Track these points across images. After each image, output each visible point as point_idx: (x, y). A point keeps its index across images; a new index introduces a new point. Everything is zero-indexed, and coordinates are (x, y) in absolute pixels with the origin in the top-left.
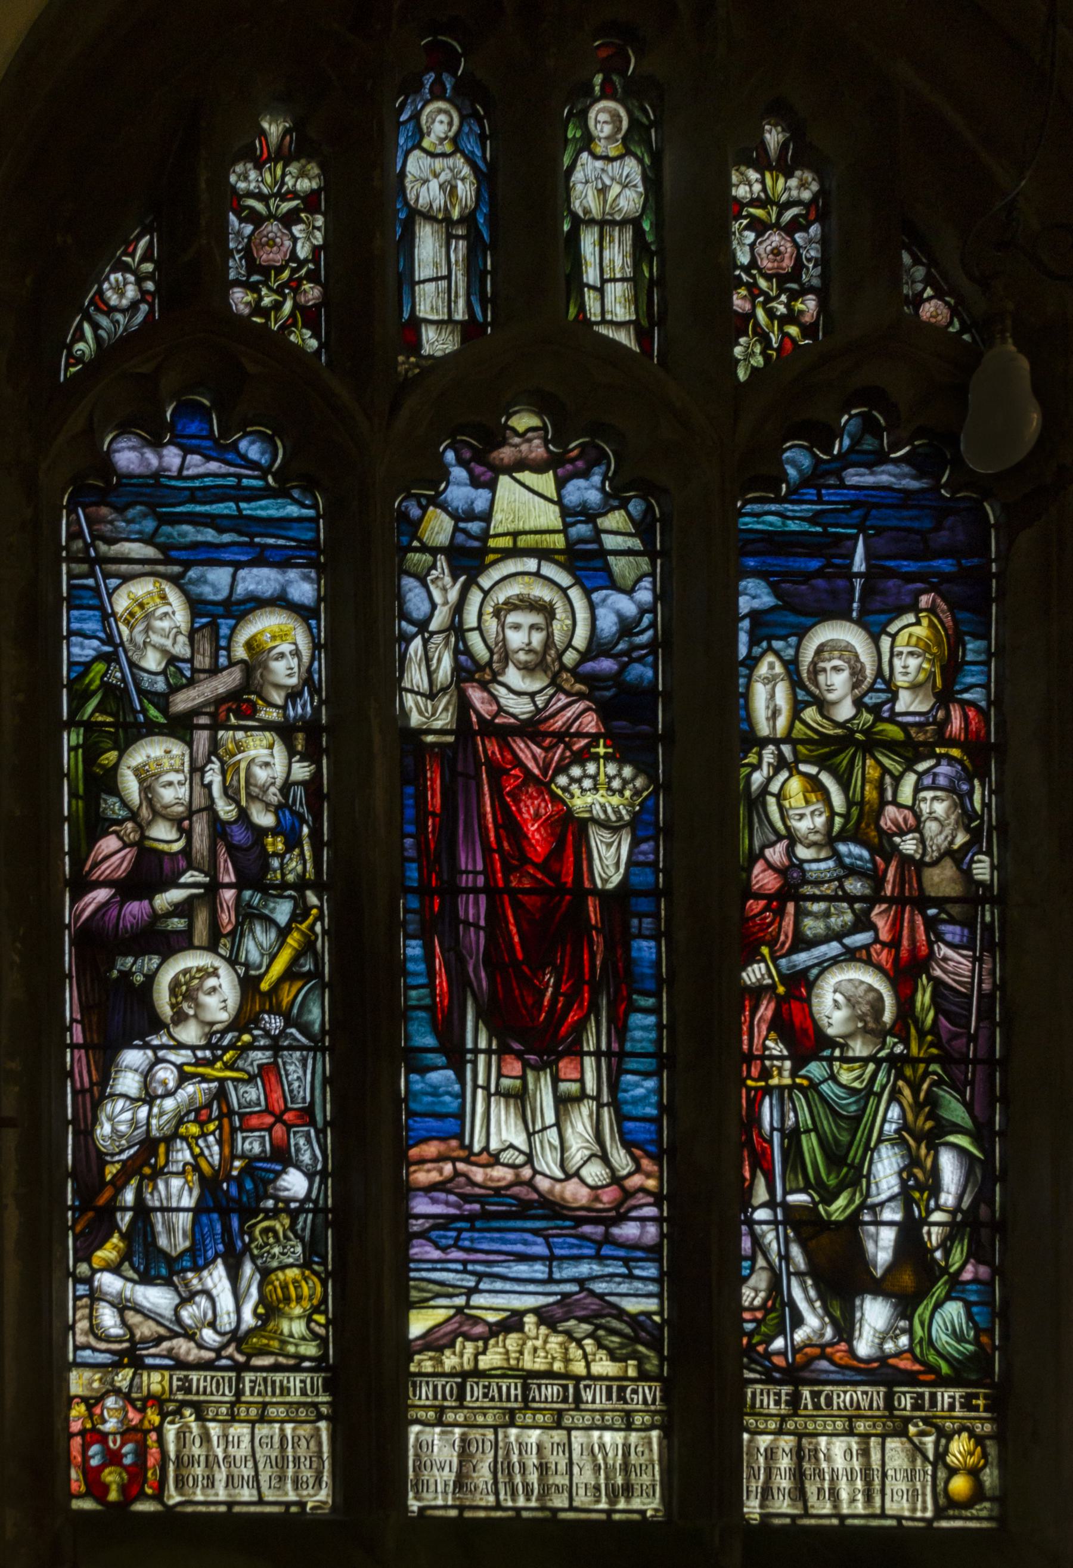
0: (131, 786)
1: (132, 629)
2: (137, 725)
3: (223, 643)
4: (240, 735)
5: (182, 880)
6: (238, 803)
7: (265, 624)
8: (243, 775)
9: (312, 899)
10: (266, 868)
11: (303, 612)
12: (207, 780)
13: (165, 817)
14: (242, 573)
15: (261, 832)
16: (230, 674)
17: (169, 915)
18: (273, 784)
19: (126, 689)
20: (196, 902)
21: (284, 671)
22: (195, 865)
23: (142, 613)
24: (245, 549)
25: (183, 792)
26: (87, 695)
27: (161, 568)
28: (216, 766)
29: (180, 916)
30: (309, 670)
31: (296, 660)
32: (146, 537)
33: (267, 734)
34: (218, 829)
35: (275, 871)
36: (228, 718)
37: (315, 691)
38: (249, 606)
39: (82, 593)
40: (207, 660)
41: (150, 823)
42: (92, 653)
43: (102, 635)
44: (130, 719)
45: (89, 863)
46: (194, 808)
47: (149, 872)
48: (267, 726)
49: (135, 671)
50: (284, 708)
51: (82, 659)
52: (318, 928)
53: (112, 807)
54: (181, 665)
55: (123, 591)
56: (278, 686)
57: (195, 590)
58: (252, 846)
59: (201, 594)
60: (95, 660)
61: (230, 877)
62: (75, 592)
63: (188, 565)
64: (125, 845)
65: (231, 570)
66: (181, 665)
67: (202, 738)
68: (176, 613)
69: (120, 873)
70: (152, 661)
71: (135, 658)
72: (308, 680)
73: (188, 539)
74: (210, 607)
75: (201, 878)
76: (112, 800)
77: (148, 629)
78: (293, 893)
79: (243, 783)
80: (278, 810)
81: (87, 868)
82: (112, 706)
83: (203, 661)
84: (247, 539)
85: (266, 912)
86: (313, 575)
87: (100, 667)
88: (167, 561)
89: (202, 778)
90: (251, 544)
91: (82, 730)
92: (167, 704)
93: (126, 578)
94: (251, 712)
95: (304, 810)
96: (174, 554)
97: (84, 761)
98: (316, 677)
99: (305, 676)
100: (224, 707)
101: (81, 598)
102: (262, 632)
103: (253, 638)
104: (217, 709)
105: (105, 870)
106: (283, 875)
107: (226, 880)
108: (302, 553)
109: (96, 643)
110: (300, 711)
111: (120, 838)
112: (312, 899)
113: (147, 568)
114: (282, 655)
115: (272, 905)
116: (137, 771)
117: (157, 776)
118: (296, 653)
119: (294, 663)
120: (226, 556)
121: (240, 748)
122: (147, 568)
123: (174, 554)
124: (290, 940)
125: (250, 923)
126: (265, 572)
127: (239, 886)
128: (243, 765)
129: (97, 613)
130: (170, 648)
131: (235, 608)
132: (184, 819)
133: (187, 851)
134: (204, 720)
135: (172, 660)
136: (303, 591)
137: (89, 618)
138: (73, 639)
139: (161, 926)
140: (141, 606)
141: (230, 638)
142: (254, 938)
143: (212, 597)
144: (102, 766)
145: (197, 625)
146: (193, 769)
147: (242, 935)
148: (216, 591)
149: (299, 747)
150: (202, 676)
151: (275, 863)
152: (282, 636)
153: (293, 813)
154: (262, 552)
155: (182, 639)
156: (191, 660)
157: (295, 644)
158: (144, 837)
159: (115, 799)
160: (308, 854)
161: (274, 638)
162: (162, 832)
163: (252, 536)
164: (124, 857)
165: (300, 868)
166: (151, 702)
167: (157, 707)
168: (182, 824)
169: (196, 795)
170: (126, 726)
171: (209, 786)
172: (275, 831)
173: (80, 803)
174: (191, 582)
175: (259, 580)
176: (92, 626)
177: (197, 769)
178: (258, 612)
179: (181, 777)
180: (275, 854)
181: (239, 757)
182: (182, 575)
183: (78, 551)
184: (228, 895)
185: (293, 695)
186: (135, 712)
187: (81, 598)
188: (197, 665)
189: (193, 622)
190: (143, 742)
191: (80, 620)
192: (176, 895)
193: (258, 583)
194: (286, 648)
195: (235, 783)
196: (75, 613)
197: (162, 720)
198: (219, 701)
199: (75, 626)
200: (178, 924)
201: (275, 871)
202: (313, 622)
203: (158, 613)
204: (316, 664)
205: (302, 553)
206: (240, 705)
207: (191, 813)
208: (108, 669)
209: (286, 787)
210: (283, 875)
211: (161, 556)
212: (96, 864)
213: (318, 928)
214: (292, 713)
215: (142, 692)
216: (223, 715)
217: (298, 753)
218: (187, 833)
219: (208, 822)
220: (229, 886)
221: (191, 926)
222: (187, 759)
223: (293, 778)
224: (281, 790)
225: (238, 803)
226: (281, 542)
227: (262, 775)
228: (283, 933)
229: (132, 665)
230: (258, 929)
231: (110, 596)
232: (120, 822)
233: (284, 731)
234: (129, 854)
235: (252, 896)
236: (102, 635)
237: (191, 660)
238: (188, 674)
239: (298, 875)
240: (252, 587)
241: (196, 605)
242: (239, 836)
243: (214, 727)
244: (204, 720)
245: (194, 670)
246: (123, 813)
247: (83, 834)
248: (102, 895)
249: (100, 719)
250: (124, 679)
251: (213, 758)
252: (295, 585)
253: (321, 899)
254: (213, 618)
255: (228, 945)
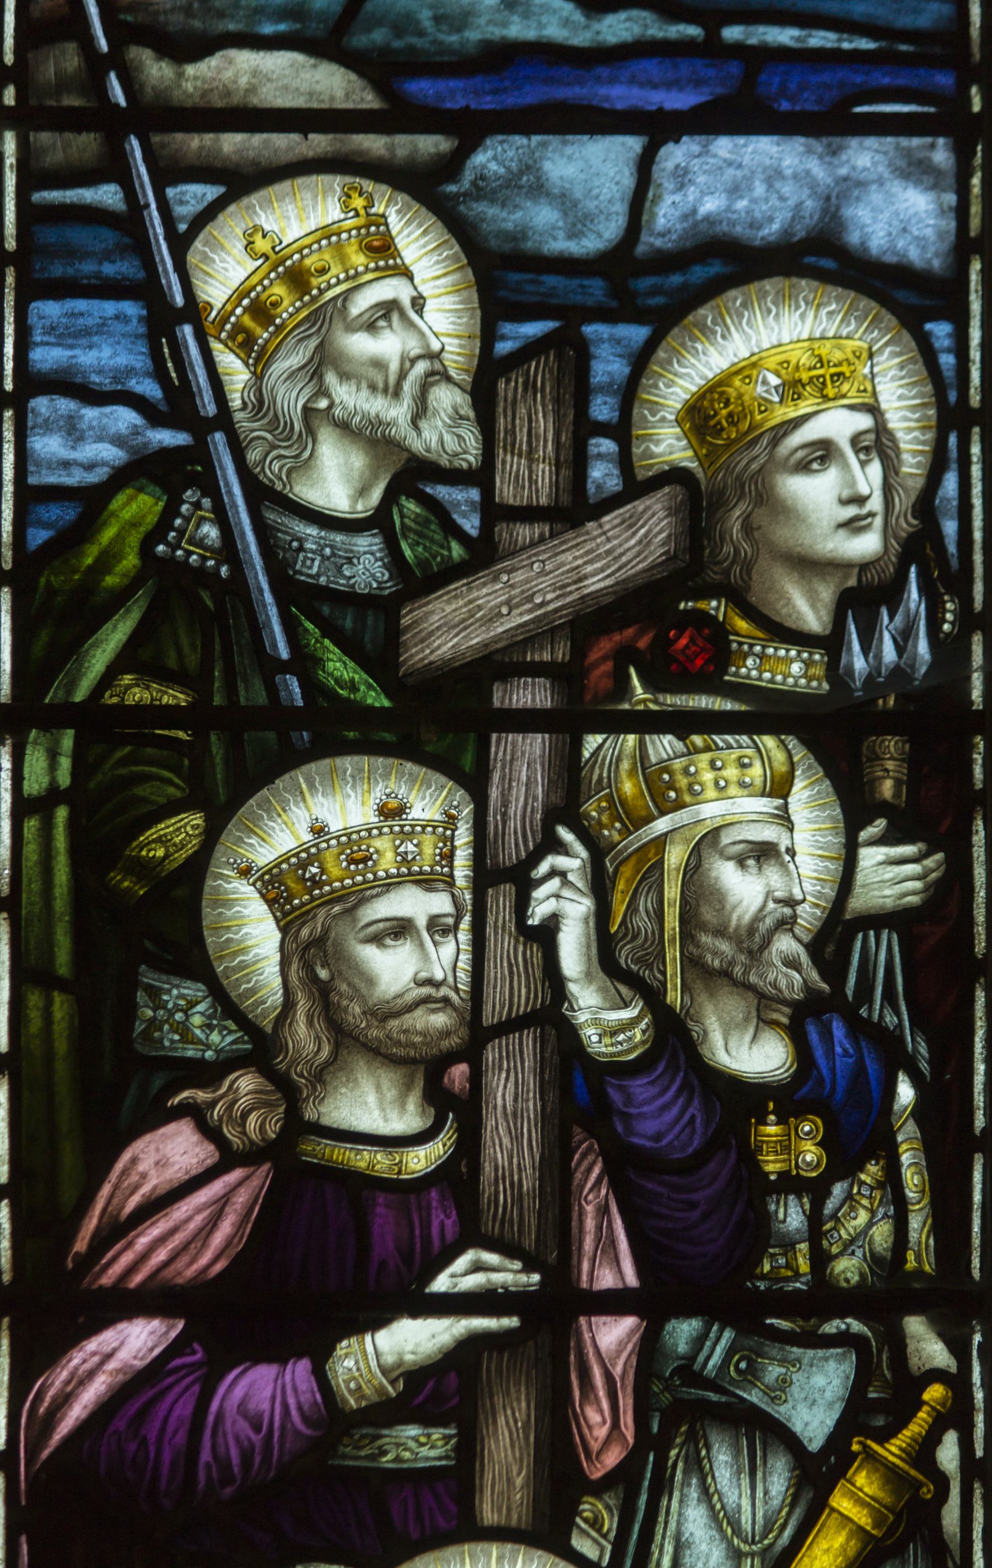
0: (254, 935)
1: (259, 361)
2: (277, 714)
3: (603, 409)
4: (663, 746)
5: (441, 1284)
6: (653, 998)
7: (764, 337)
8: (672, 891)
9: (928, 1347)
10: (758, 1233)
11: (901, 294)
12: (539, 912)
13: (383, 1055)
14: (675, 155)
15: (743, 1100)
16: (630, 524)
17: (387, 1412)
18: (786, 924)
19: (239, 584)
20: (489, 1364)
21: (832, 508)
22: (490, 1227)
23: (301, 304)
24: (685, 68)
25: (448, 958)
26: (90, 612)
27: (374, 144)
28: (574, 861)
29: (427, 1421)
30: (925, 506)
31: (875, 469)
32: (315, 29)
33: (769, 742)
34: (578, 1089)
35: (789, 1245)
36: (623, 689)
37: (946, 580)
38: (699, 273)
39: (78, 235)
40: (544, 473)
41: (321, 1077)
42: (111, 454)
43: (150, 389)
44: (253, 694)
45: (91, 1224)
46: (489, 1017)
47: (322, 1247)
48: (769, 713)
49: (271, 516)
50: (832, 643)
51: (74, 478)
52: (948, 1454)
53: (184, 1017)
54: (442, 492)
55: (231, 227)
56: (810, 566)
57: (496, 218)
58: (701, 1158)
59: (521, 234)
60: (122, 477)
61: (617, 1271)
62: (48, 235)
63: (470, 130)
64: (229, 1156)
65: (634, 144)
66: (442, 492)
67: (523, 763)
68: (426, 300)
69: (209, 1259)
70: (335, 481)
71: (272, 471)
72: (919, 544)
73: (473, 35)
74: (552, 281)
75: (508, 1275)
76: (182, 991)
77: (324, 361)
78: (856, 1326)
79: (672, 921)
80: (800, 1020)
81: (81, 1245)
82: (185, 647)
83: (528, 477)
84: (693, 31)
85: (754, 1397)
86: (942, 155)
87: (138, 506)
88: (398, 116)
89: (522, 904)
90: (710, 48)
91: (67, 740)
92: (393, 638)
93: (242, 182)
94: (710, 659)
95: (897, 1019)
96: (422, 89)
97: (73, 851)
98: (950, 528)
99: (907, 525)
100: (605, 646)
101: (72, 254)
102: (746, 370)
103: (715, 389)
104: (579, 651)
105: (148, 1251)
106: (820, 1259)
107: (606, 1280)
108: (903, 80)
109: (124, 418)
110: (889, 653)
111: (209, 1132)
112: (928, 1347)
113: (320, 143)
114: (824, 452)
115: (774, 1372)
116: (274, 886)
117: (353, 899)
118: (877, 443)
119: (870, 478)
120: (620, 94)
121: (664, 793)
122: (322, 143)
123: (422, 89)
124: (841, 1502)
125: (693, 1438)
126: (763, 149)
127: (651, 1304)
128: (675, 856)
129: (131, 309)
130: (403, 430)
131: (645, 283)
132: (451, 1058)
133: (460, 1174)
134: (530, 695)
135: (412, 475)
136: (902, 213)
137: (101, 328)
138: (41, 405)
139: (352, 1455)
140: (298, 279)
141: (629, 392)
142: (706, 1494)
143: (560, 245)
144: (143, 869)
145: (503, 348)
146: (486, 875)
147: (661, 1486)
148: (578, 223)
149: (887, 788)
150: (524, 532)
151: (792, 1216)
152: (818, 381)
153: (861, 1029)
154: (749, 79)
155: (446, 398)
156: (482, 476)
157: (873, 410)
158: (298, 1127)
159: (193, 989)
160: (912, 1181)
161: (792, 388)
162: (370, 1106)
163: (713, 20)
164: (224, 1200)
165: (882, 1234)
166: (330, 630)
167: (351, 648)
168: (445, 1081)
169: (495, 971)
170: (236, 722)
171: (546, 935)
172: (785, 1098)
173: (61, 1006)
174: (482, 189)
175: (738, 179)
176: (112, 352)
177: (502, 876)
178: (735, 296)
179: (440, 903)
180: (790, 1183)
181: (662, 825)
182: (452, 166)
183: (63, 84)
184: (613, 1334)
185: (865, 596)
186: (271, 668)
187: (72, 254)
188: (506, 492)
189: (488, 335)
190: (299, 776)
191: (67, 335)
192: (413, 1339)
193: (735, 190)
194: (839, 424)
195: (642, 921)
196: (48, 310)
197: (376, 699)
198: (590, 621)
199: (46, 357)
200: (419, 1445)
201: (789, 1245)
202: (940, 331)
203: (362, 302)
204: (950, 483)
205: (903, 80)
206: (669, 639)
207: (477, 1035)
208: (171, 511)
209: (838, 931)
210: (820, 1259)
211: (369, 100)
212: (118, 1230)
213: (948, 1454)
214: (859, 664)
215: (296, 595)
216: (600, 676)
217: (883, 809)
218: (456, 1110)
219: (542, 1064)
220: (613, 1303)
221: (468, 1451)
222: (463, 836)
223: (859, 902)
224: (815, 948)
225: (653, 998)
226: (821, 39)
227: (745, 890)
228: (817, 1476)
229: (261, 494)
230: (722, 1461)
231: (180, 245)
232: (210, 1073)
233: (833, 731)
234: (244, 1188)
235: (699, 1341)
236: (150, 389)
237: (482, 476)
238: (471, 525)
239: (875, 1260)
240: (710, 205)
241: (499, 274)
242: (657, 1117)
243: (566, 724)
244: (530, 695)
245: (492, 511)
246: (222, 1039)
247: (66, 1116)
248: (136, 1340)
249: (137, 695)
250: (229, 548)
251: (566, 835)
252: (876, 196)
253: (959, 1348)
254: (561, 320)
255: (610, 1523)
